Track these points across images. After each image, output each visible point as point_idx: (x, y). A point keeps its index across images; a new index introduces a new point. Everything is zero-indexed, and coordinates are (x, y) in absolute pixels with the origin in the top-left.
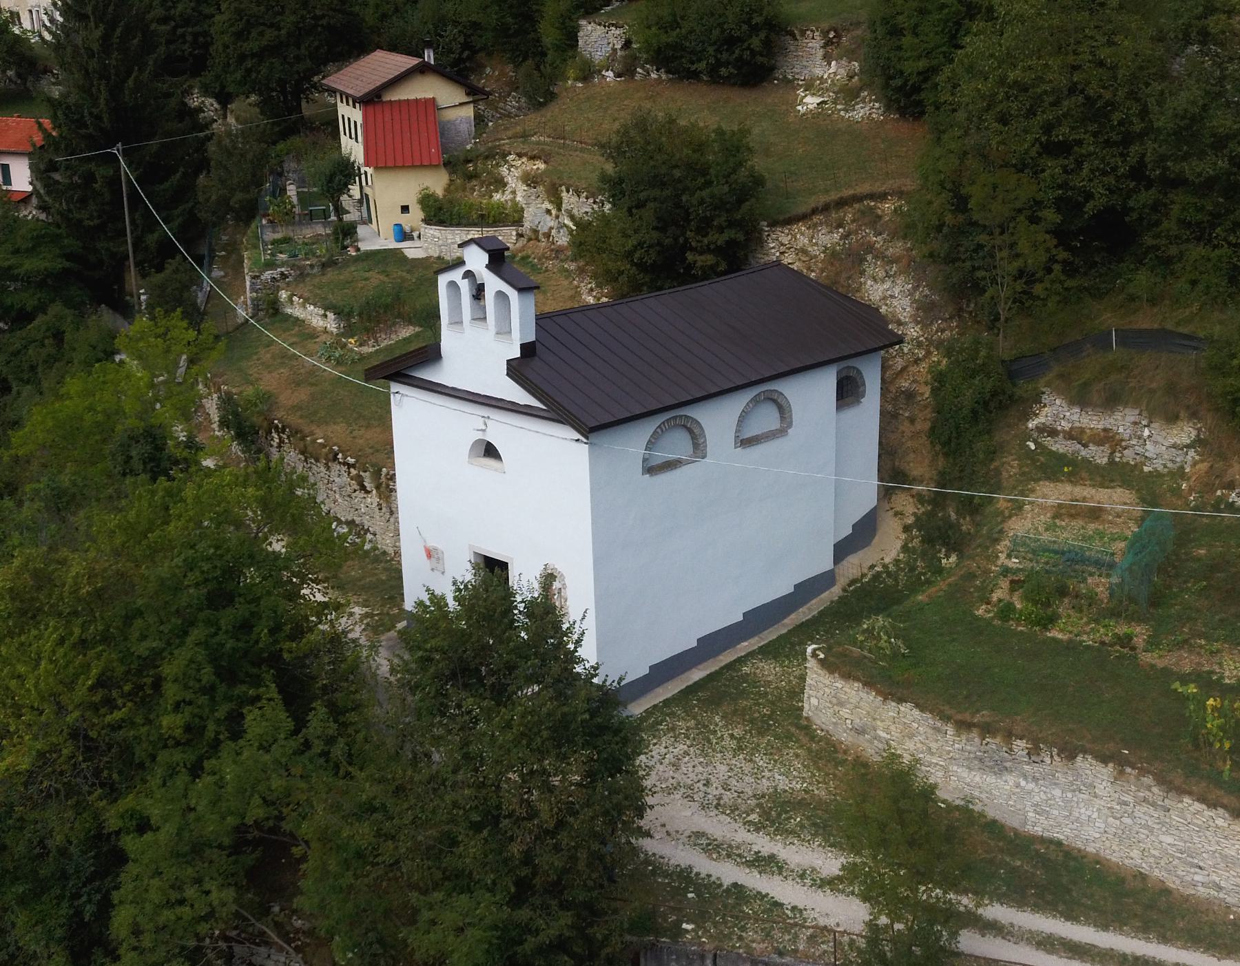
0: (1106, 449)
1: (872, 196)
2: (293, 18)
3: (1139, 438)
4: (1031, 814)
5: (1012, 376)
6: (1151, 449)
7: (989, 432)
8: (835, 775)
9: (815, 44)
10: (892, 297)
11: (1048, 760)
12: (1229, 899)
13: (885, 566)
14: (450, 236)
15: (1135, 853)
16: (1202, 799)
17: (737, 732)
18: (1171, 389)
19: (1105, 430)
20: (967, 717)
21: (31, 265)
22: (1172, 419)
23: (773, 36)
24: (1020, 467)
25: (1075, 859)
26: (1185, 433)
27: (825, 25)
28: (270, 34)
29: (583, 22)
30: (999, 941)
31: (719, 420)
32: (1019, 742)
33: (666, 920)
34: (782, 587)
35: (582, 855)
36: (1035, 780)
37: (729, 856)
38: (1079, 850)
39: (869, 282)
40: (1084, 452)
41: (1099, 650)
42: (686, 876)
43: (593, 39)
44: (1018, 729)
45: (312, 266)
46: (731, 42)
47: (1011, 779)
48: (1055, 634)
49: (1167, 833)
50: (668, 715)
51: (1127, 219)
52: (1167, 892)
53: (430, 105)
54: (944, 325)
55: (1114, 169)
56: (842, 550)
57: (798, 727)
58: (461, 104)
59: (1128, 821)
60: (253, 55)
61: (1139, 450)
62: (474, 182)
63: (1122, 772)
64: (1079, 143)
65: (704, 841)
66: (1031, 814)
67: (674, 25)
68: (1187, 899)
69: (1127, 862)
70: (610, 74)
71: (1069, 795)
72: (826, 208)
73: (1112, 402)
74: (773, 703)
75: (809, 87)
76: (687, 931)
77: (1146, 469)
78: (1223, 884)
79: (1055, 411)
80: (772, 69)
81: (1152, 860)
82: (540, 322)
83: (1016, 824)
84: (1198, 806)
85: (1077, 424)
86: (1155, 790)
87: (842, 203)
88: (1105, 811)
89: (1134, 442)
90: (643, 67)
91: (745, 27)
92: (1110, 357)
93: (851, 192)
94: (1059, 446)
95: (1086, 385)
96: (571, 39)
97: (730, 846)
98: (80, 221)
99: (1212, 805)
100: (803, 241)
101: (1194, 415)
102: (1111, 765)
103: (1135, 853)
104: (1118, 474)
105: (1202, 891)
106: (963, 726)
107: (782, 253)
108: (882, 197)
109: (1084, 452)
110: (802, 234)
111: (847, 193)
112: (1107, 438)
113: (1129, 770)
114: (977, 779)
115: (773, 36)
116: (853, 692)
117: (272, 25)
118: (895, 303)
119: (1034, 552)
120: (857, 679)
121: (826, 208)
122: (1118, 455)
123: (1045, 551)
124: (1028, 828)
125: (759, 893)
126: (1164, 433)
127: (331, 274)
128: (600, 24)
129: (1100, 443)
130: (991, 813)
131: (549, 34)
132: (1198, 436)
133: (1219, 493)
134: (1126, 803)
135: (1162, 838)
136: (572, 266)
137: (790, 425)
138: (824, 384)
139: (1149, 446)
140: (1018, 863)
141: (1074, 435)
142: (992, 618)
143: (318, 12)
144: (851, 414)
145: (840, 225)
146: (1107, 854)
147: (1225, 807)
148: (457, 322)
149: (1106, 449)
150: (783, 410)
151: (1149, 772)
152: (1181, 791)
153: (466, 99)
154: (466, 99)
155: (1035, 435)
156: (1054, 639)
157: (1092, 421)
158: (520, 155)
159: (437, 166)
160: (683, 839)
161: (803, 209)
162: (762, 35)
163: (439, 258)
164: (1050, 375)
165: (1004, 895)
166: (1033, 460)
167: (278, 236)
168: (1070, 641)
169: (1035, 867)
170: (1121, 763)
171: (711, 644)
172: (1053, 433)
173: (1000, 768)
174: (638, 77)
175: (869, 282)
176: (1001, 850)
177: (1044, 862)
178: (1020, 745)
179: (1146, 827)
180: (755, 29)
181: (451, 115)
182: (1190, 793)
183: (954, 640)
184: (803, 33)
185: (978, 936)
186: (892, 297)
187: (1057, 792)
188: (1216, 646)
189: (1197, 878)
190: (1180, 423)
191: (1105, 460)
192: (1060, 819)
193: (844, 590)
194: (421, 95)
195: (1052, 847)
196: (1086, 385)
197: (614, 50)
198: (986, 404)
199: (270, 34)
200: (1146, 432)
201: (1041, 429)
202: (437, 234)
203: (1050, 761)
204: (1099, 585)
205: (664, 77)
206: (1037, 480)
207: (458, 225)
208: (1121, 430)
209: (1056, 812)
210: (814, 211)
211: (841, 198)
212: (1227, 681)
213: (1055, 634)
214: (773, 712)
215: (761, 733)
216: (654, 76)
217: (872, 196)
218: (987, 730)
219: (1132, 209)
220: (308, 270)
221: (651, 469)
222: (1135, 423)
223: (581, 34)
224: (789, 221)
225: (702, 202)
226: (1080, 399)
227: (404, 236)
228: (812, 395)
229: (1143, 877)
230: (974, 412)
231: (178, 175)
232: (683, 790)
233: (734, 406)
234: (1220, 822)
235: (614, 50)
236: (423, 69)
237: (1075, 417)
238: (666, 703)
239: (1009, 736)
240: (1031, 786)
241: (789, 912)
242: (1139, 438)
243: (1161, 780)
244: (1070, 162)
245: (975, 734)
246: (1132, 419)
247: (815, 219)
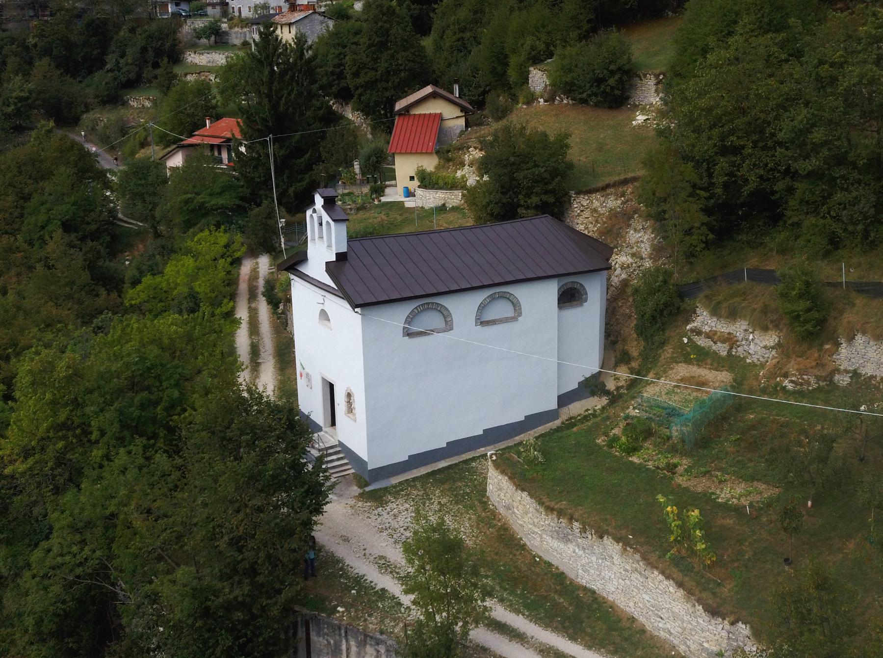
0: (726, 346)
2: (386, 65)
3: (747, 340)
4: (580, 571)
5: (681, 295)
6: (752, 348)
7: (663, 330)
8: (485, 533)
10: (642, 242)
11: (590, 537)
12: (675, 642)
13: (595, 411)
15: (631, 604)
16: (663, 573)
17: (444, 501)
18: (765, 310)
19: (729, 334)
20: (552, 504)
21: (221, 201)
22: (765, 329)
23: (625, 78)
24: (673, 353)
25: (598, 603)
26: (771, 339)
27: (657, 71)
28: (371, 74)
29: (532, 69)
30: (518, 646)
31: (463, 308)
33: (330, 604)
34: (518, 416)
35: (262, 554)
36: (584, 549)
37: (391, 572)
38: (604, 598)
39: (632, 232)
41: (654, 471)
42: (358, 581)
44: (576, 515)
45: (351, 209)
46: (599, 81)
47: (571, 547)
48: (635, 459)
49: (646, 593)
50: (411, 486)
51: (773, 198)
52: (643, 631)
53: (439, 117)
54: (666, 261)
55: (766, 165)
56: (564, 400)
57: (481, 502)
58: (457, 117)
59: (628, 582)
60: (362, 86)
61: (746, 347)
62: (451, 164)
63: (625, 550)
64: (743, 147)
65: (383, 562)
66: (580, 571)
67: (570, 71)
68: (652, 637)
69: (628, 609)
70: (542, 100)
71: (600, 561)
72: (615, 185)
73: (733, 315)
74: (475, 486)
75: (644, 111)
76: (339, 612)
77: (748, 361)
78: (672, 631)
79: (704, 320)
80: (628, 98)
81: (639, 610)
82: (350, 243)
83: (573, 577)
84: (661, 577)
85: (714, 329)
86: (641, 563)
87: (625, 182)
88: (618, 574)
89: (744, 343)
90: (559, 97)
91: (605, 72)
92: (742, 285)
93: (633, 175)
94: (702, 342)
95: (719, 303)
96: (525, 79)
97: (395, 567)
98: (253, 178)
99: (668, 578)
100: (596, 204)
101: (777, 327)
102: (621, 544)
103: (631, 604)
104: (732, 363)
105: (663, 634)
106: (550, 509)
107: (582, 211)
110: (597, 200)
111: (630, 175)
112: (730, 340)
113: (628, 549)
114: (555, 545)
115: (625, 78)
116: (504, 481)
117: (373, 69)
118: (643, 245)
119: (651, 407)
120: (506, 474)
121: (615, 185)
122: (734, 350)
123: (659, 407)
124: (579, 580)
125: (393, 596)
126: (761, 338)
127: (361, 215)
131: (513, 75)
132: (779, 341)
133: (778, 379)
134: (626, 570)
135: (644, 596)
137: (520, 314)
138: (549, 292)
139: (752, 346)
140: (562, 600)
142: (604, 446)
143: (400, 62)
144: (572, 313)
145: (623, 195)
146: (618, 602)
147: (673, 579)
148: (313, 239)
149: (726, 346)
150: (516, 305)
151: (639, 551)
152: (653, 566)
155: (689, 333)
159: (431, 153)
160: (372, 558)
161: (600, 184)
162: (617, 77)
164: (702, 295)
165: (541, 619)
166: (682, 349)
167: (346, 191)
168: (640, 464)
169: (570, 604)
170: (626, 543)
171: (455, 447)
173: (566, 539)
174: (556, 102)
175: (632, 232)
176: (556, 592)
177: (578, 603)
179: (636, 587)
180: (612, 73)
181: (450, 124)
182: (657, 568)
183: (574, 457)
184: (645, 76)
185: (507, 641)
186: (642, 242)
187: (594, 559)
188: (727, 477)
189: (660, 625)
190: (770, 332)
191: (725, 353)
192: (595, 576)
193: (563, 423)
195: (589, 594)
196: (719, 303)
198: (662, 311)
199: (371, 74)
200: (751, 337)
201: (692, 330)
202: (421, 193)
203: (591, 538)
204: (675, 431)
205: (571, 102)
206: (677, 363)
207: (432, 188)
209: (593, 571)
210: (608, 186)
211: (626, 179)
212: (720, 500)
213: (635, 459)
214: (472, 491)
215: (457, 503)
216: (565, 102)
218: (560, 513)
219: (776, 192)
221: (409, 334)
222: (746, 330)
224: (590, 192)
225: (525, 178)
226: (715, 312)
227: (409, 194)
228: (539, 299)
229: (633, 620)
230: (654, 318)
231: (308, 155)
232: (390, 531)
233: (476, 299)
234: (671, 589)
235: (546, 86)
237: (713, 324)
238: (414, 479)
239: (571, 519)
240: (581, 553)
241: (403, 610)
242: (747, 340)
243: (644, 558)
244: (737, 159)
246: (744, 327)
247: (609, 191)
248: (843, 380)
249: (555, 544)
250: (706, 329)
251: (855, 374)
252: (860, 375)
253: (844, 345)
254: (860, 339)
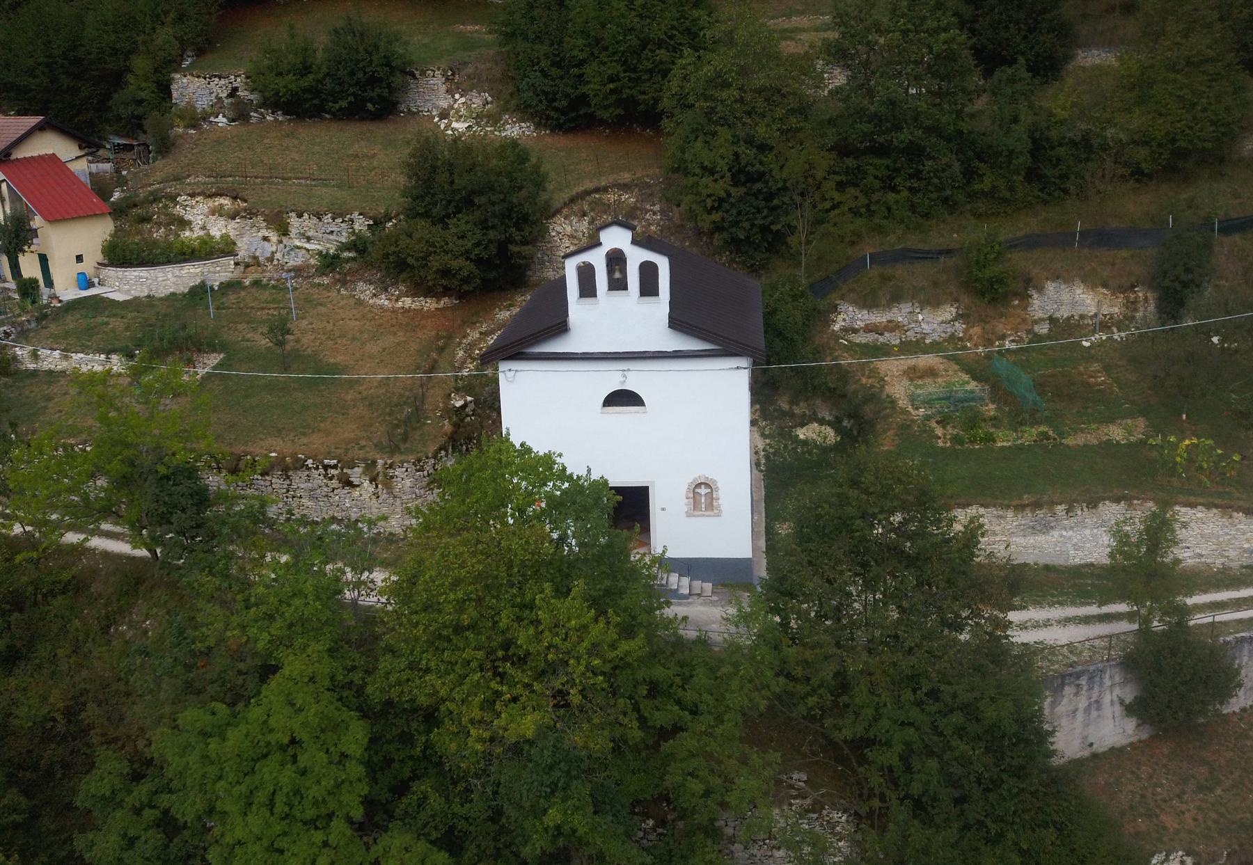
1: (597, 190)
9: (437, 81)
11: (1079, 513)
12: (1209, 561)
14: (161, 274)
19: (889, 321)
26: (949, 312)
32: (1059, 507)
36: (1072, 528)
40: (881, 339)
43: (190, 90)
47: (1056, 533)
53: (53, 158)
58: (77, 158)
61: (918, 330)
73: (896, 298)
77: (927, 341)
90: (256, 111)
94: (861, 339)
106: (1020, 508)
108: (605, 190)
109: (881, 339)
112: (893, 327)
128: (198, 77)
129: (892, 330)
130: (1042, 561)
136: (326, 280)
141: (869, 329)
153: (80, 153)
154: (80, 153)
156: (1002, 447)
157: (878, 318)
158: (192, 195)
159: (103, 214)
163: (149, 296)
172: (855, 331)
173: (1047, 528)
174: (253, 121)
178: (1060, 509)
184: (423, 73)
187: (1087, 532)
194: (42, 152)
197: (219, 99)
200: (920, 317)
203: (1081, 513)
208: (900, 319)
217: (597, 190)
218: (1037, 505)
220: (27, 326)
223: (174, 87)
226: (869, 302)
234: (1199, 515)
236: (40, 128)
237: (866, 317)
239: (1052, 504)
240: (1071, 533)
245: (1028, 512)
248: (1043, 329)
249: (1031, 540)
250: (860, 324)
251: (1052, 320)
252: (1057, 320)
253: (1035, 296)
254: (1050, 287)
